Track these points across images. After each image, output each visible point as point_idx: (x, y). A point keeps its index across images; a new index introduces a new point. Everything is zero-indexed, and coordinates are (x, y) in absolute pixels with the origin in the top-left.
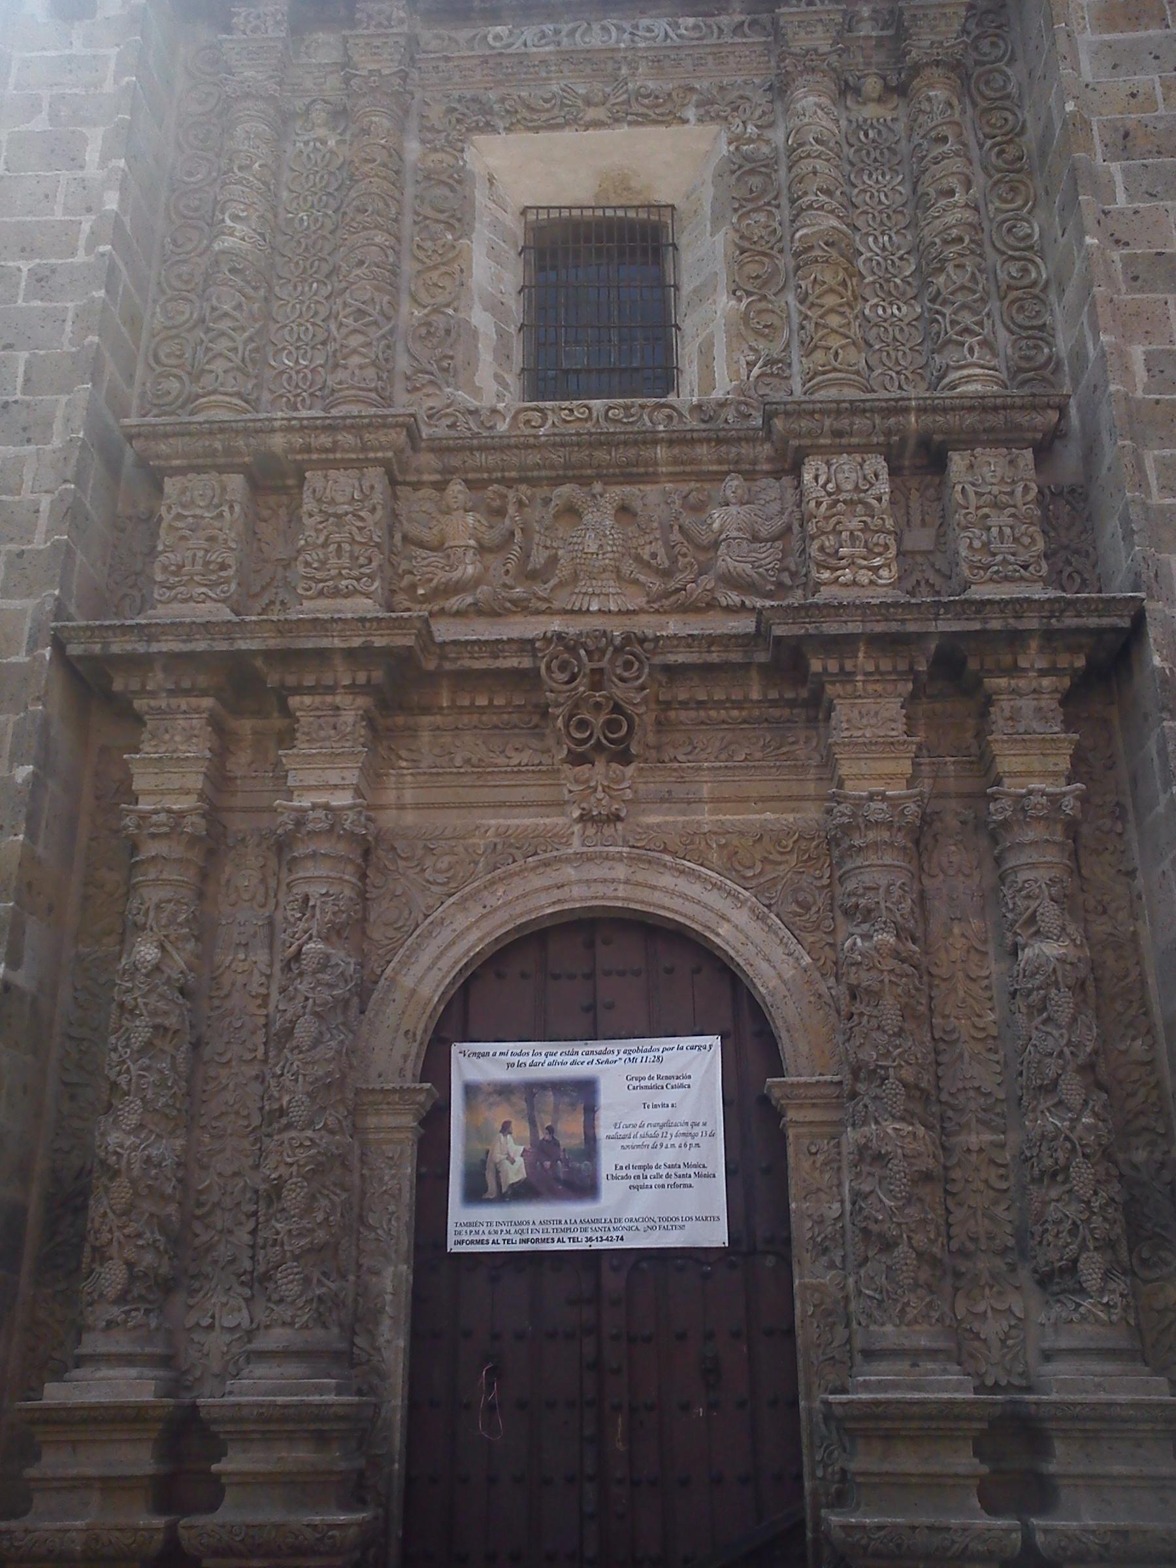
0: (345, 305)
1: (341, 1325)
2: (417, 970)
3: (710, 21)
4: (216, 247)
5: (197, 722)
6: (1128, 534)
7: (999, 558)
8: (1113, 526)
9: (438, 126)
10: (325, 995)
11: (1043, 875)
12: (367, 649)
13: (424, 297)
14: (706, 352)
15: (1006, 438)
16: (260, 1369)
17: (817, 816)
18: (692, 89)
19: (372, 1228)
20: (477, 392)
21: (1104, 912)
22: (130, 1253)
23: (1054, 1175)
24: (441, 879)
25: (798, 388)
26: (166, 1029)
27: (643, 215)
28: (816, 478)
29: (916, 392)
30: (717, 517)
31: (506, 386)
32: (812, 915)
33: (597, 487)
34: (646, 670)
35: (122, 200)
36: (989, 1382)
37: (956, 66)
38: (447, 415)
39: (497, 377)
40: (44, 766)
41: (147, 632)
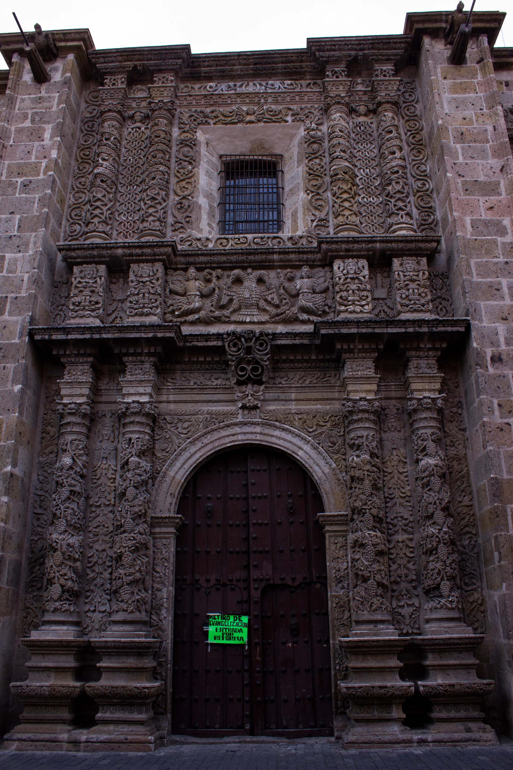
0: (147, 195)
1: (146, 611)
2: (175, 469)
3: (297, 82)
4: (96, 171)
5: (86, 367)
6: (464, 293)
7: (412, 302)
8: (458, 289)
9: (186, 122)
10: (139, 479)
11: (429, 431)
12: (155, 338)
13: (179, 192)
14: (294, 215)
15: (416, 253)
16: (115, 628)
17: (338, 406)
18: (290, 109)
19: (158, 572)
20: (200, 231)
21: (454, 445)
22: (62, 581)
23: (432, 551)
24: (185, 431)
25: (332, 231)
26: (75, 492)
27: (269, 158)
28: (339, 268)
29: (379, 233)
30: (299, 283)
31: (212, 228)
32: (336, 447)
33: (249, 270)
34: (269, 347)
35: (58, 153)
36: (405, 631)
37: (396, 104)
38: (188, 241)
39: (209, 224)
40: (25, 385)
41: (66, 330)
